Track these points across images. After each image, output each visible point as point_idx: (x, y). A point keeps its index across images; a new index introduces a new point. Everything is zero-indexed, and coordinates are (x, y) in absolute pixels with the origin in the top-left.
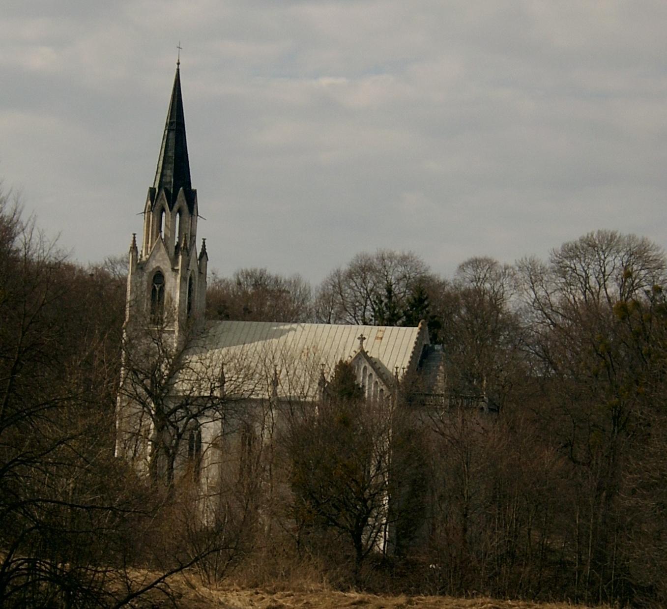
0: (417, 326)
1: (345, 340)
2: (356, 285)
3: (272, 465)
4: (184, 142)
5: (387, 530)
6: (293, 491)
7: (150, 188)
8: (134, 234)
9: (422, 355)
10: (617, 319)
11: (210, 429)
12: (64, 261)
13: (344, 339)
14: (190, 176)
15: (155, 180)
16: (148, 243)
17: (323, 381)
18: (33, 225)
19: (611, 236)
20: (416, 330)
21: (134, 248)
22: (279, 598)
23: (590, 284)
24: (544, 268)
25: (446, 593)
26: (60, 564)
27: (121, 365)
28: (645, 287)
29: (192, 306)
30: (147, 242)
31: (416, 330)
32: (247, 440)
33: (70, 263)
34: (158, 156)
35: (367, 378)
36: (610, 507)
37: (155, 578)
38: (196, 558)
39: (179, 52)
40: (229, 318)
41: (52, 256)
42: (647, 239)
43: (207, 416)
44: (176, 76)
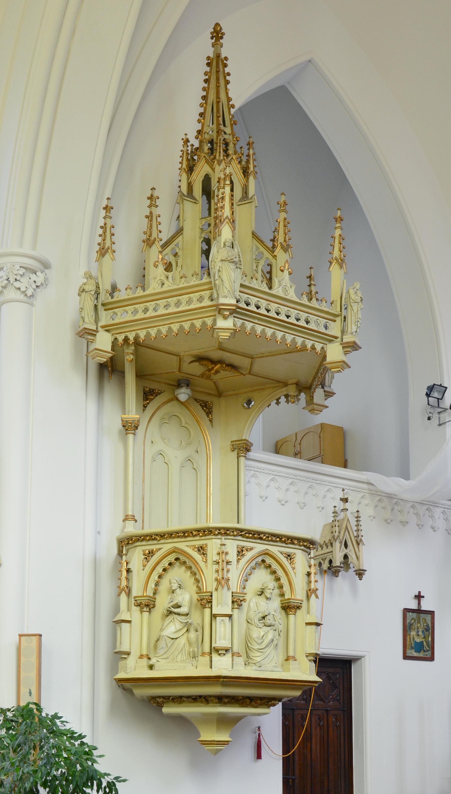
0: (112, 350)
3: (25, 722)
5: (225, 680)
7: (406, 611)
11: (291, 780)
13: (243, 182)
16: (224, 685)
20: (316, 678)
21: (181, 622)
22: (2, 721)
24: (420, 526)
26: (78, 765)
29: (122, 641)
31: (316, 678)
33: (176, 456)
34: (170, 355)
35: (430, 627)
36: (76, 757)
37: (209, 319)
43: (155, 593)
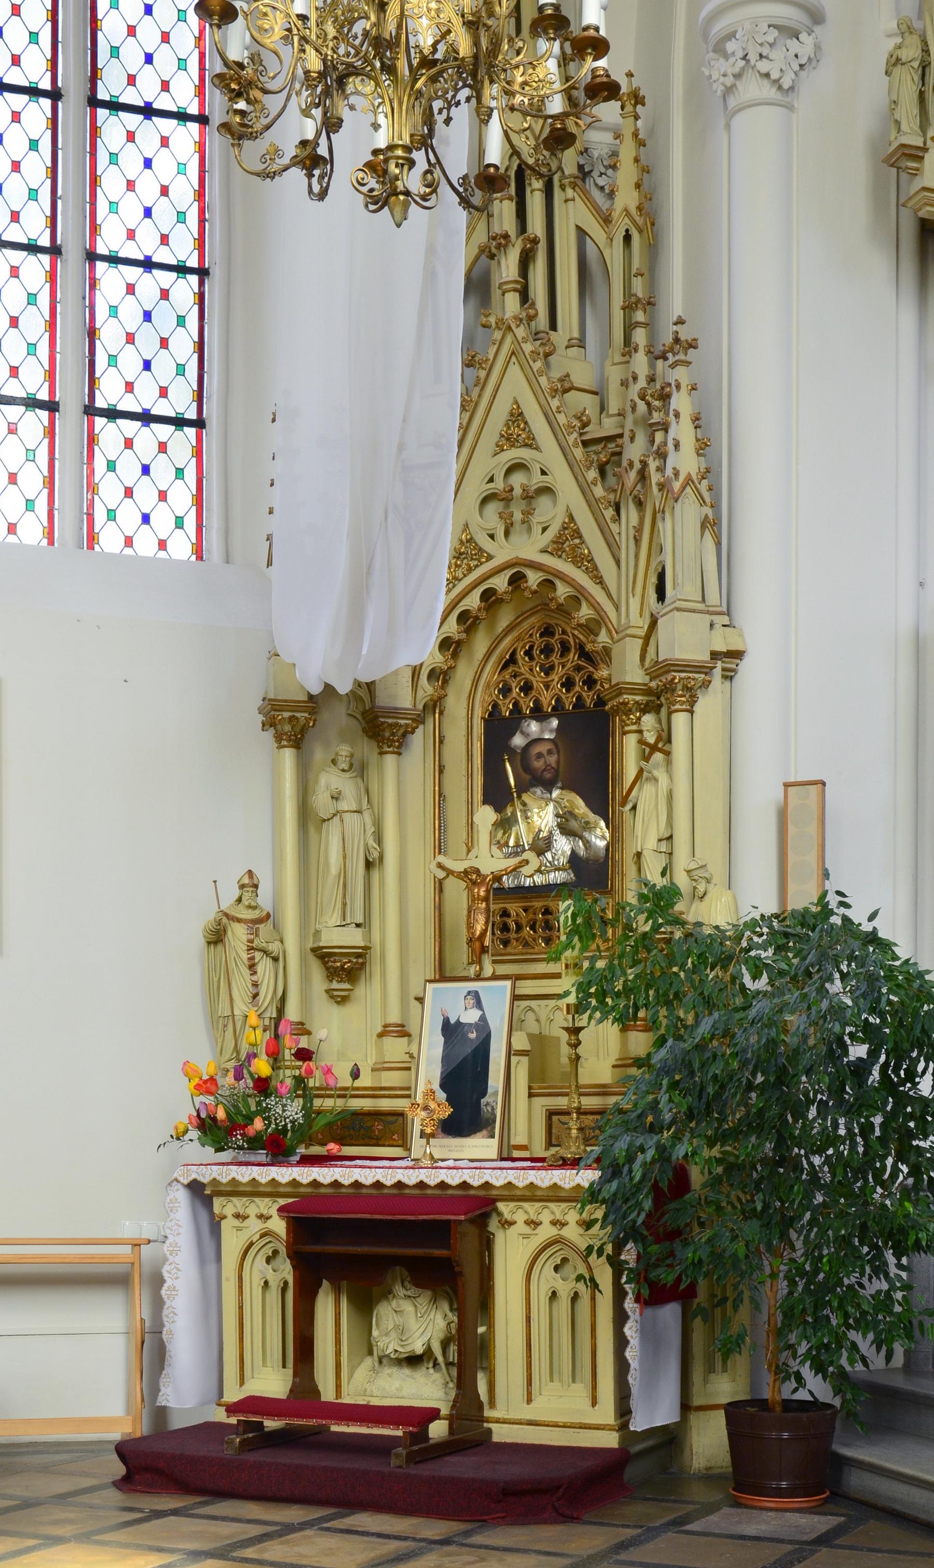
1: (398, 12)
2: (566, 357)
4: (361, 1142)
6: (578, 1185)
8: (215, 882)
9: (588, 804)
10: (354, 83)
12: (494, 1427)
14: (541, 1445)
15: (496, 390)
17: (896, 945)
18: (517, 618)
19: (401, 1311)
23: (433, 141)
25: (209, 1100)
27: (856, 1135)
28: (663, 965)
30: (226, 960)
32: (696, 676)
38: (868, 1204)
39: (540, 1028)
40: (468, 366)
41: (494, 263)
42: (207, 1086)
44: (900, 249)
